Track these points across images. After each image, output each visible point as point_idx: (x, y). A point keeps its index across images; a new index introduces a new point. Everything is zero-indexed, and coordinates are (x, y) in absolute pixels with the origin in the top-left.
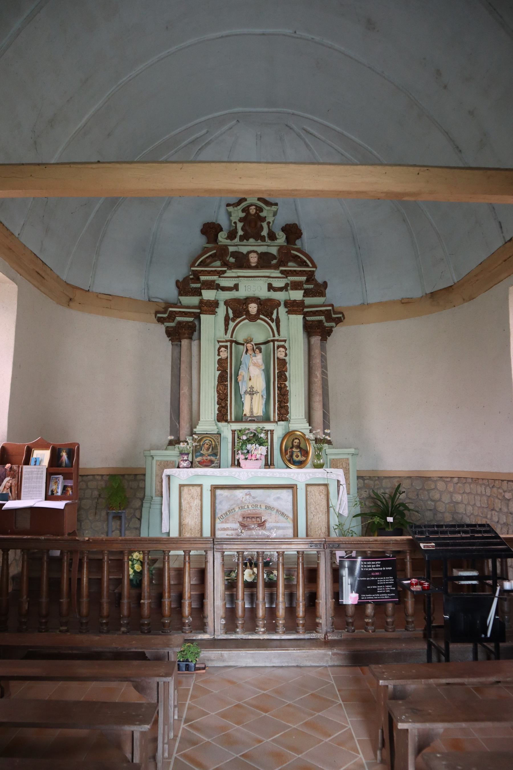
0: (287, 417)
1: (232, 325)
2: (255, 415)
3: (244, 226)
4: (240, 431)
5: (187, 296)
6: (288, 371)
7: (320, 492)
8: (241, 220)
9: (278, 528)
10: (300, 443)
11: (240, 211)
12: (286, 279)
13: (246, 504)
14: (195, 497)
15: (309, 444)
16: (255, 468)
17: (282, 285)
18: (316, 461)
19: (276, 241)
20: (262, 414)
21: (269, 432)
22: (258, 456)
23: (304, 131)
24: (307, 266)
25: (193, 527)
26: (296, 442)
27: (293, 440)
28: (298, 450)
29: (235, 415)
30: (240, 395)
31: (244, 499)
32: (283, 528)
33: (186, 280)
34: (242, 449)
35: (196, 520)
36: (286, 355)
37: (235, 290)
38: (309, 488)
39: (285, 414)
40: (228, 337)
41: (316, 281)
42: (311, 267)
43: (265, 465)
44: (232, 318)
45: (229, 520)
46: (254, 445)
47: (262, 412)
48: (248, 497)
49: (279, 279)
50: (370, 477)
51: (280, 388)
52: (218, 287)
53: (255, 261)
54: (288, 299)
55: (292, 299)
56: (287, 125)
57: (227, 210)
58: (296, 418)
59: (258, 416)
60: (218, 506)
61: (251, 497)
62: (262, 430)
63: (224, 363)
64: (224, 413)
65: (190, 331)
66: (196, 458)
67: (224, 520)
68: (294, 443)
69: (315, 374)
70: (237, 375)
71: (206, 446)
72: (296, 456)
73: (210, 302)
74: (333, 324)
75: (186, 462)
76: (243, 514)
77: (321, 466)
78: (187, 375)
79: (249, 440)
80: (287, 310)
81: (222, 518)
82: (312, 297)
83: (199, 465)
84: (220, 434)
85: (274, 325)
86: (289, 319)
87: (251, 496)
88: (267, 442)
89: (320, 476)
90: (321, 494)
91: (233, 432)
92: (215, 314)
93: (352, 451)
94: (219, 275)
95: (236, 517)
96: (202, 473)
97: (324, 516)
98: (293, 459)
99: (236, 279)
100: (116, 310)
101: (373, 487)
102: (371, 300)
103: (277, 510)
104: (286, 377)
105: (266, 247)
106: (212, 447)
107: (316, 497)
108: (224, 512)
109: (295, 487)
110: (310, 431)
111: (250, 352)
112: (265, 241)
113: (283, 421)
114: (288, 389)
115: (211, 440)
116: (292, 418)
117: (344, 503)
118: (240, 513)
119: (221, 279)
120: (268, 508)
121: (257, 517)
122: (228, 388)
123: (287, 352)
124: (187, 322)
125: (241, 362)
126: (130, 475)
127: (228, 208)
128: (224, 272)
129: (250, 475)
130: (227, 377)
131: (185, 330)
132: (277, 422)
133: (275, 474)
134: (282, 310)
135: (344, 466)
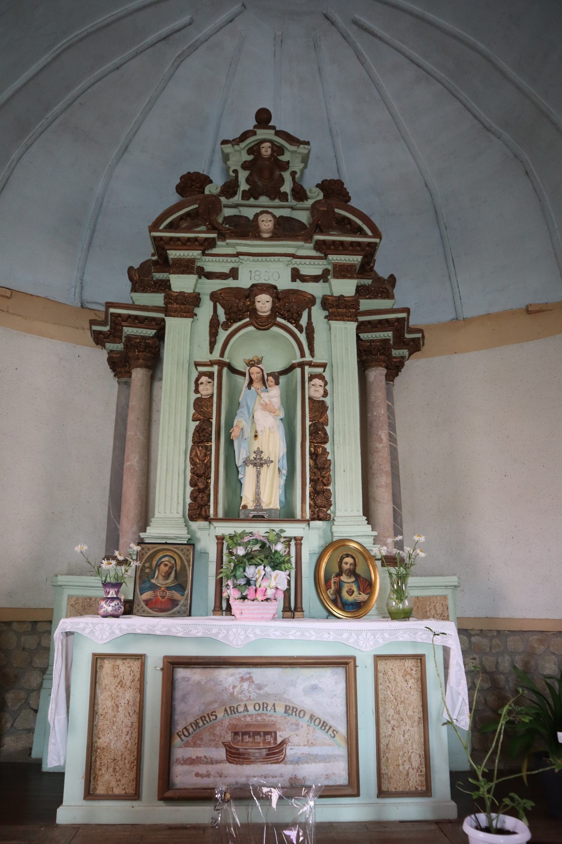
0: (329, 512)
1: (223, 335)
2: (264, 506)
3: (250, 175)
4: (231, 537)
5: (146, 292)
6: (329, 423)
7: (406, 674)
8: (245, 166)
9: (315, 758)
10: (355, 564)
11: (244, 153)
12: (325, 262)
13: (242, 700)
14: (128, 683)
15: (374, 567)
16: (262, 619)
17: (318, 272)
18: (394, 603)
19: (305, 202)
20: (278, 507)
21: (293, 543)
22: (270, 593)
23: (355, 28)
24: (365, 235)
25: (120, 753)
26: (346, 563)
27: (342, 559)
28: (353, 579)
29: (224, 507)
30: (235, 469)
31: (236, 690)
32: (325, 759)
33: (145, 267)
34: (235, 576)
35: (128, 738)
36: (325, 394)
37: (231, 278)
38: (382, 665)
39: (325, 507)
40: (216, 356)
41: (376, 273)
42: (370, 237)
43: (284, 610)
44: (224, 322)
45: (201, 739)
46: (262, 567)
47: (278, 502)
48: (245, 685)
49: (312, 261)
50: (481, 630)
51: (314, 456)
52: (202, 273)
53: (270, 227)
54: (328, 293)
55: (335, 295)
56: (326, 17)
57: (222, 149)
58: (346, 514)
59: (271, 510)
60: (179, 707)
61: (253, 686)
62: (278, 536)
63: (207, 407)
64: (202, 503)
65: (148, 355)
66: (141, 594)
67: (190, 738)
68: (344, 565)
69: (377, 435)
70: (230, 425)
71: (164, 569)
72: (347, 592)
73: (184, 296)
74: (405, 352)
75: (113, 604)
76: (235, 726)
77: (405, 615)
78: (138, 433)
79: (250, 557)
80: (326, 313)
81: (186, 734)
82: (370, 298)
83: (146, 608)
84: (193, 545)
85: (302, 337)
86: (330, 329)
87: (253, 682)
88: (289, 561)
89: (406, 637)
90: (408, 677)
91: (220, 539)
92: (193, 318)
93: (453, 580)
94: (202, 248)
95: (217, 732)
96: (145, 630)
97: (416, 729)
98: (341, 598)
99: (234, 259)
100: (18, 315)
101: (488, 650)
102: (468, 314)
103: (312, 717)
104: (326, 434)
105: (289, 210)
106: (176, 570)
107: (397, 686)
108: (192, 720)
109: (352, 663)
110: (374, 540)
111: (257, 385)
112: (287, 201)
113: (320, 519)
114: (329, 457)
115: (176, 557)
116: (337, 514)
117: (461, 699)
118: (226, 723)
119: (207, 258)
120: (290, 712)
121: (266, 733)
122: (211, 454)
123: (328, 388)
124: (143, 338)
125: (239, 403)
126: (24, 622)
127: (223, 146)
128: (211, 243)
129: (251, 635)
130: (211, 431)
131: (139, 351)
132: (308, 521)
133: (306, 634)
134: (318, 314)
135: (439, 611)
